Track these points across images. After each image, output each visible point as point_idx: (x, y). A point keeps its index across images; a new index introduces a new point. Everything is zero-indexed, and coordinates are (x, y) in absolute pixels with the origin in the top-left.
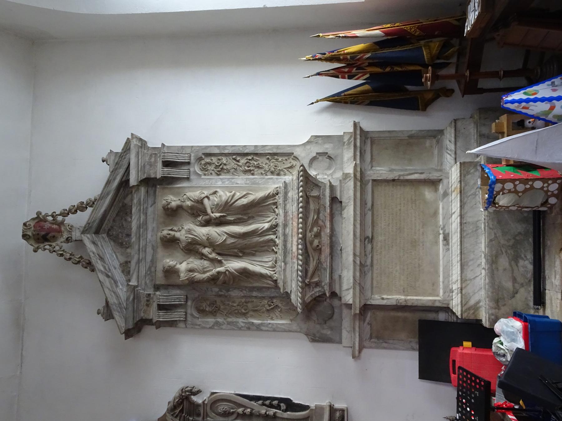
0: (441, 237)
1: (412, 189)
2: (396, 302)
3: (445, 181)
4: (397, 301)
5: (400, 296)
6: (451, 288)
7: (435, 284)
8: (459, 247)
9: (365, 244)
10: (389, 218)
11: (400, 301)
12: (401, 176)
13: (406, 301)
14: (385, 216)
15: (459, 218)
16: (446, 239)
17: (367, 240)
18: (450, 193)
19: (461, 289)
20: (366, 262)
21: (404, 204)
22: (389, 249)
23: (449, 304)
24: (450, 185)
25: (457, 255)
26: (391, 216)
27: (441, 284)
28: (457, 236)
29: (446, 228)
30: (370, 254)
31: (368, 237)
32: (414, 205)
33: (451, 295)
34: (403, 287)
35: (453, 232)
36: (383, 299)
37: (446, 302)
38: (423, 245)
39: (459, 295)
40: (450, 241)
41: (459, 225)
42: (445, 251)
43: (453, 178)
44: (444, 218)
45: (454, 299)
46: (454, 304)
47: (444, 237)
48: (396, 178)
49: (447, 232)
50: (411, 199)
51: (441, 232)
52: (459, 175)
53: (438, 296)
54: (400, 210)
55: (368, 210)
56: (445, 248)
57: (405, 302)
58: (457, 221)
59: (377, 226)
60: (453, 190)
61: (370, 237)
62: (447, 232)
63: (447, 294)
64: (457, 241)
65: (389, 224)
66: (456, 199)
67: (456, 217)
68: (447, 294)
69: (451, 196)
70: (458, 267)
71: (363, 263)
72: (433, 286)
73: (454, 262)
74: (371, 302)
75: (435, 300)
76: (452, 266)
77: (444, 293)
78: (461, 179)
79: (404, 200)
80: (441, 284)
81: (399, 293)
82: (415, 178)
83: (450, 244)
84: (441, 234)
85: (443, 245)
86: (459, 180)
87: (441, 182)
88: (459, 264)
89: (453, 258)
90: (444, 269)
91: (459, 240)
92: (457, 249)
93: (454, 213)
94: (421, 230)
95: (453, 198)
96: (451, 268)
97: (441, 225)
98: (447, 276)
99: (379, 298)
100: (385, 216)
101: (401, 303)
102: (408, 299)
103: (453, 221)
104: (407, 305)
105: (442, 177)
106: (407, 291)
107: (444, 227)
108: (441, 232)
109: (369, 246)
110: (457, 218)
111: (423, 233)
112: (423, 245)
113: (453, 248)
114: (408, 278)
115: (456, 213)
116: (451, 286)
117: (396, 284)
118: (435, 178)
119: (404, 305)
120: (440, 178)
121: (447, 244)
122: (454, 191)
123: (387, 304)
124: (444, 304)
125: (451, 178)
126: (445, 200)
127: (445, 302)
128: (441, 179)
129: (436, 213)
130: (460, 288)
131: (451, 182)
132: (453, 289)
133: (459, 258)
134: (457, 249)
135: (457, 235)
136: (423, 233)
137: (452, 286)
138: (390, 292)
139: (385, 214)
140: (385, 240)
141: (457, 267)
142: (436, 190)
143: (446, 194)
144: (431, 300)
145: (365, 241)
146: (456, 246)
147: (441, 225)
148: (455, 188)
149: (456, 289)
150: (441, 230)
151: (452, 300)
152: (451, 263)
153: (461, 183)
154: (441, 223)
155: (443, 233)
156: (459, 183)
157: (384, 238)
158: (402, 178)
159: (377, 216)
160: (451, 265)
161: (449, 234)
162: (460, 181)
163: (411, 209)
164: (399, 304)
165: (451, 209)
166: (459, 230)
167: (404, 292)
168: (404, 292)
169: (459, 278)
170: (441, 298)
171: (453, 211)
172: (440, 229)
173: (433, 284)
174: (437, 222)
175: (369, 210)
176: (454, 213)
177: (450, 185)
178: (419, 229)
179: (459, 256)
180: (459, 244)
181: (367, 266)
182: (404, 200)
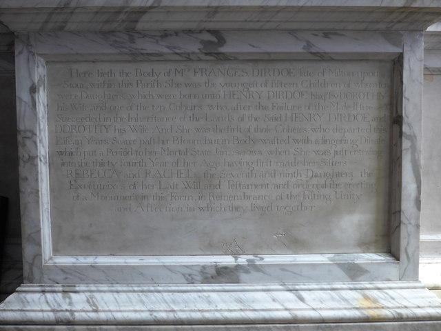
0: (227, 260)
1: (369, 175)
2: (25, 131)
3: (393, 269)
4: (29, 134)
5: (46, 141)
6: (77, 289)
7: (89, 243)
8: (197, 316)
9: (201, 31)
10: (281, 108)
11: (28, 142)
12: (412, 141)
13: (33, 159)
14: (289, 96)
15: (285, 315)
16: (222, 275)
17: (214, 39)
18: (358, 286)
19: (68, 323)
20: (144, 36)
21: (324, 153)
22: (186, 108)
23: (31, 281)
24: (380, 285)
25: (173, 311)
26: (289, 114)
27: (90, 260)
28: (231, 311)
29: (255, 274)
30: (168, 47)
31: (222, 41)
32: (322, 181)
33: (57, 289)
34: (74, 150)
35: (241, 295)
36: (33, 90)
37: (37, 275)
38: (201, 209)
39: (51, 316)
40: (217, 287)
41: (266, 315)
42: (187, 271)
43: (405, 293)
44: (283, 267)
45: (43, 297)
46: (29, 296)
47: (226, 268)
48: (405, 129)
49: (243, 276)
50: (339, 175)
51: (243, 260)
52: (420, 312)
53: (56, 251)
54: (307, 141)
55: (308, 42)
56: (195, 272)
57: (27, 156)
58: (277, 310)
59: (256, 72)
60: (367, 292)
61: (223, 50)
62: (243, 276)
63: (60, 277)
64: (217, 311)
65: (265, 108)
66: (344, 305)
67: (290, 306)
68: (60, 277)
69: (351, 289)
70: (136, 311)
71: (139, 26)
72: (82, 237)
73: (152, 296)
74: (20, 53)
75: (39, 244)
76: (142, 292)
77: (64, 270)
78: (408, 319)
79: (336, 152)
80: (90, 260)
81: (55, 140)
82: (403, 185)
83: (206, 287)
84: (236, 259)
85: (204, 267)
86: (404, 312)
87: (390, 259)
88: (145, 316)
89: (165, 294)
90: (133, 268)
91: (218, 315)
92: (191, 311)
93: (302, 299)
94: (247, 203)
95: (343, 293)
96: (136, 289)
97: (262, 259)
98: (112, 277)
99: (36, 79)
100: (289, 96)
101: (24, 145)
102: (36, 166)
103: (276, 294)
104: (21, 163)
105: (406, 260)
106: (63, 164)
107: (258, 268)
108: (243, 260)
109: (193, 47)
110: (286, 309)
111: (237, 209)
112: (201, 209)
113: (195, 295)
114: (102, 164)
115: (302, 305)
116: (82, 287)
117: (82, 128)
118: (403, 243)
119: (20, 154)
120: (403, 256)
121: (206, 278)
122: (366, 298)
123: (18, 104)
124: (31, 269)
125: (401, 288)
126: (339, 272)
127: (36, 270)
128: (398, 259)
129: (297, 245)
130: (71, 319)
131: (390, 288)
132: (72, 295)
133: (163, 316)
134: (191, 311)
135: (235, 310)
136: (237, 209)
137: (83, 292)
138: (58, 111)
139: (293, 95)
140: (213, 96)
141: (137, 308)
142: (364, 246)
143: (354, 272)
144: (39, 231)
145: (209, 31)
146: (200, 306)
147: (262, 259)
148: (375, 301)
149: (70, 304)
150: (248, 261)
151: (43, 292)
152: (152, 288)
153: (394, 320)
154: (269, 259)
155: (238, 267)
156: (396, 316)
157: (222, 94)
158: (406, 144)
159: (289, 73)
160: (145, 288)
161: (237, 281)
162: (400, 319)
163: (310, 174)
164: (20, 138)
165: (310, 287)
166: (251, 315)
167: (61, 153)
168: (407, 325)
169: (103, 316)
170: (51, 258)
171: (304, 294)
172: (251, 257)
173: (87, 238)
174: (272, 248)
175: (309, 45)
176: (302, 299)
177: (380, 285)
178: (249, 198)
179: (171, 316)
180: (208, 315)
181: (132, 40)
182: (336, 152)
